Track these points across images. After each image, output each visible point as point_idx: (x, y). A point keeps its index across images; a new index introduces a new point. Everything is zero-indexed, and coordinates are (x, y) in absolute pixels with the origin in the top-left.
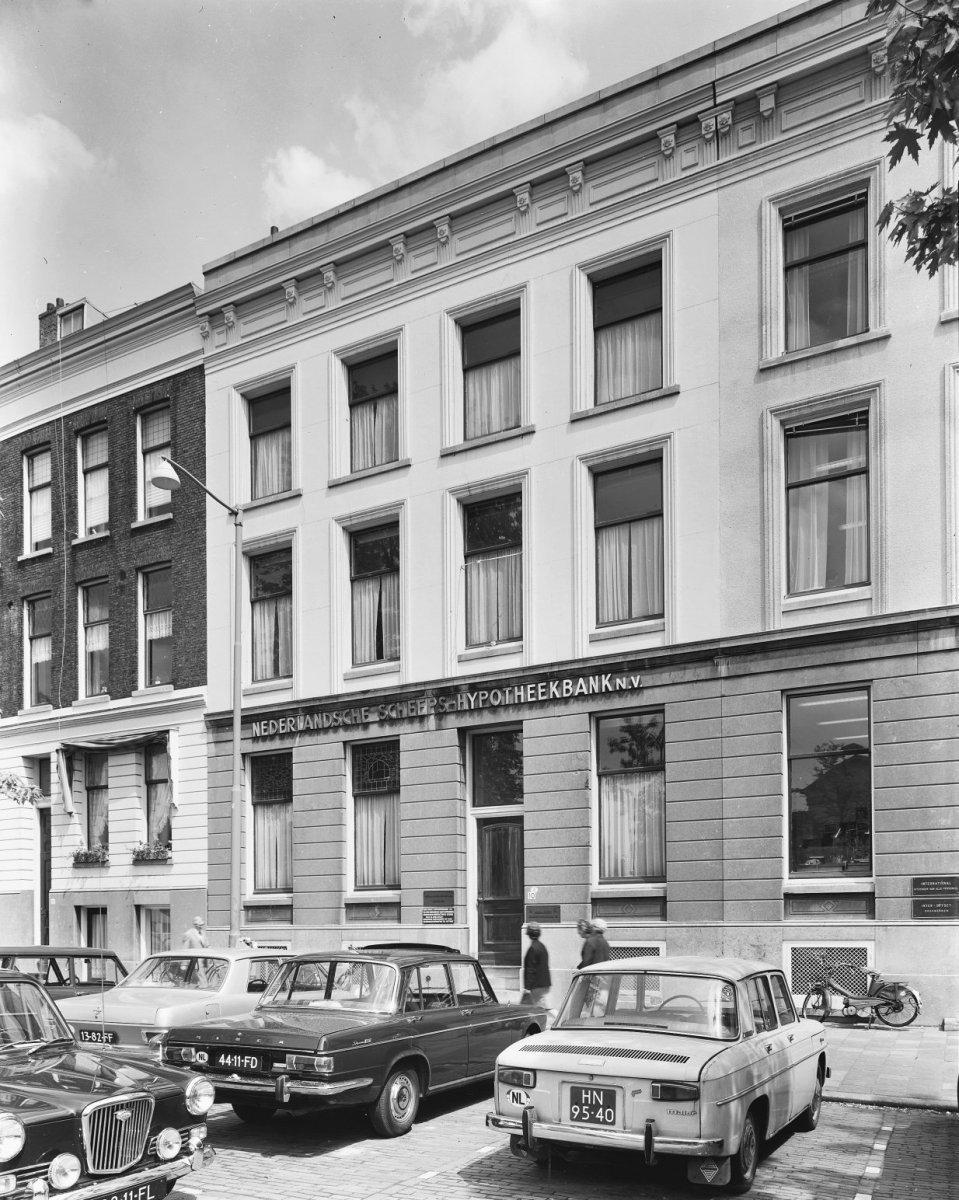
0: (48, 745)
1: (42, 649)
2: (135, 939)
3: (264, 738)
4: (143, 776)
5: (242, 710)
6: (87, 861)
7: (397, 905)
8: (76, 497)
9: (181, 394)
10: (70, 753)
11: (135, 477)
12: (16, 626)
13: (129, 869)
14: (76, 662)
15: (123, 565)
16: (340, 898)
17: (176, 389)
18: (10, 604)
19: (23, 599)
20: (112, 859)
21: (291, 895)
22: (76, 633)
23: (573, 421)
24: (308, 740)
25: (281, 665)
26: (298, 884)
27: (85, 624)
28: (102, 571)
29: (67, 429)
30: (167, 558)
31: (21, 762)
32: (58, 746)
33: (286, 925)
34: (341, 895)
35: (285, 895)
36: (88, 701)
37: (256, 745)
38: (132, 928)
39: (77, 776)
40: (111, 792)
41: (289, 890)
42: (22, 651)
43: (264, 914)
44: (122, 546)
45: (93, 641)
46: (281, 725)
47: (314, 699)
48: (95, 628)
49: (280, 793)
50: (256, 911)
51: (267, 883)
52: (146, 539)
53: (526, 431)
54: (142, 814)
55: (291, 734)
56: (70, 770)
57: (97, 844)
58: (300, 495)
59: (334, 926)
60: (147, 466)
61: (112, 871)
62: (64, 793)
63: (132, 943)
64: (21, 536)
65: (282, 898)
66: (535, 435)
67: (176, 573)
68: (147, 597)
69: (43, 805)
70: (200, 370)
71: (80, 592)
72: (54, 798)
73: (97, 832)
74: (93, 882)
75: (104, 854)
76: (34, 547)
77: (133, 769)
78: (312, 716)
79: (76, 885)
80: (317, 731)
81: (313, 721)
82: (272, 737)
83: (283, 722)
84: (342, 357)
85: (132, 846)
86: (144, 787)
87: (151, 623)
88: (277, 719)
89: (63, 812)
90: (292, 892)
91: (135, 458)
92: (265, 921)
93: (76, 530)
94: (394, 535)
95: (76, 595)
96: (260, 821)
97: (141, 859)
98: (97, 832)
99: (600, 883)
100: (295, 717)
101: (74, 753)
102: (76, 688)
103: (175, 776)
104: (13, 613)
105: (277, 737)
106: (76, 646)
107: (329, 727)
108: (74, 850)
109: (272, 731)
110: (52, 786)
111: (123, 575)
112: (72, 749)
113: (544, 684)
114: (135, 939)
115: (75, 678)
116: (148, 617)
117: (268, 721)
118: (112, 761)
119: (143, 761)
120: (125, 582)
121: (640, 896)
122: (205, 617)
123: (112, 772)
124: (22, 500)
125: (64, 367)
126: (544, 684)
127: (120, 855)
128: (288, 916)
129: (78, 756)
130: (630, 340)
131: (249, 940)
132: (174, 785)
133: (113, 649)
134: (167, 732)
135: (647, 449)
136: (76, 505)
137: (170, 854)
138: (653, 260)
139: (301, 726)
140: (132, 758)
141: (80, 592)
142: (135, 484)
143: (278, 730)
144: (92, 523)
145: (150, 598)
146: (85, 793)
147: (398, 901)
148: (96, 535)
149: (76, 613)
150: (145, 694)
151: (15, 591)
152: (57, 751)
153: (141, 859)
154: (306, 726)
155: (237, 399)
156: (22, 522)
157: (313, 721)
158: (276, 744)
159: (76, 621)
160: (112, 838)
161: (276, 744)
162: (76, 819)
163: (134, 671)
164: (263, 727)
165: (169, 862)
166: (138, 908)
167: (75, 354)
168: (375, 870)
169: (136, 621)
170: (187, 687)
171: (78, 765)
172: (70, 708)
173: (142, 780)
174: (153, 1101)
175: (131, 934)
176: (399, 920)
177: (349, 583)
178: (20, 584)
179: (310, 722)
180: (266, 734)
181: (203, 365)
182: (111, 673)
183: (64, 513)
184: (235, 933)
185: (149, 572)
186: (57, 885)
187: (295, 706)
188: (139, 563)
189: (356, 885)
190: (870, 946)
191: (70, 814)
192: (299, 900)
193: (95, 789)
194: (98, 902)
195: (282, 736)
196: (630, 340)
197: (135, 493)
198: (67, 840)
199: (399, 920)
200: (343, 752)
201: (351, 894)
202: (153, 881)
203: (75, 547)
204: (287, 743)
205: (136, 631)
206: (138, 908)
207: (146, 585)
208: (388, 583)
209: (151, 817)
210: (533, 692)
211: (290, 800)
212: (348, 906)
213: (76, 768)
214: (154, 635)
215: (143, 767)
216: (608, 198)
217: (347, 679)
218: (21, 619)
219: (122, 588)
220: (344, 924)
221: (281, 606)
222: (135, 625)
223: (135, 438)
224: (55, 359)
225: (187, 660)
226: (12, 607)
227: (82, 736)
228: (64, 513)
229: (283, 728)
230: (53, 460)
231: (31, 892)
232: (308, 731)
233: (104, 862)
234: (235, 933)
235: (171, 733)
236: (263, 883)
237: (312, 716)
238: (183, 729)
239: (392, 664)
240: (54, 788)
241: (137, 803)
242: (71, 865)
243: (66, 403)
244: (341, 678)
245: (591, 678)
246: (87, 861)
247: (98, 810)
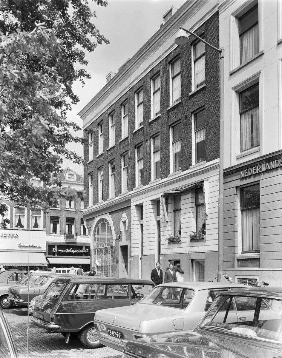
0: (158, 195)
1: (158, 156)
2: (191, 274)
3: (246, 178)
4: (172, 208)
5: (224, 170)
6: (174, 241)
7: (258, 259)
8: (169, 90)
9: (209, 28)
10: (167, 196)
11: (191, 73)
12: (148, 149)
13: (188, 244)
14: (169, 159)
15: (186, 113)
16: (234, 257)
17: (207, 27)
18: (147, 140)
19: (151, 137)
20: (183, 240)
21: (259, 253)
22: (169, 146)
23: (278, 44)
24: (267, 175)
25: (254, 142)
26: (263, 248)
27: (172, 142)
28: (178, 118)
29: (166, 63)
30: (203, 104)
31: (150, 202)
32: (162, 194)
33: (257, 269)
34: (235, 255)
35: (256, 253)
36: (173, 173)
37: (242, 181)
38: (190, 270)
39: (170, 206)
40: (182, 212)
41: (258, 251)
42: (151, 158)
43: (246, 263)
44: (185, 105)
45: (175, 149)
46: (254, 170)
47: (270, 154)
48: (176, 143)
49: (254, 204)
50: (243, 261)
51: (248, 248)
52: (195, 99)
53: (261, 54)
54: (194, 220)
55: (259, 174)
56: (167, 204)
57: (177, 233)
58: (263, 54)
59: (232, 269)
60: (196, 67)
61: (182, 245)
62: (166, 214)
63: (190, 275)
64: (150, 112)
65: (255, 255)
66: (264, 55)
67: (207, 110)
68: (196, 124)
69: (158, 219)
70: (217, 12)
71: (171, 129)
72: (161, 216)
73: (177, 229)
74: (176, 250)
75: (179, 238)
76: (196, 87)
77: (190, 200)
78: (269, 163)
79: (169, 251)
80: (272, 170)
81: (270, 165)
82: (250, 177)
83: (255, 168)
84: (235, 15)
85: (189, 234)
86: (195, 208)
87: (198, 134)
88: (252, 167)
89: (164, 222)
90: (260, 252)
91: (191, 65)
92: (247, 266)
93: (169, 104)
94: (257, 89)
95: (169, 131)
96: (245, 219)
97: (193, 239)
98: (177, 229)
99: (242, 253)
100: (261, 165)
101: (168, 196)
102: (169, 169)
103: (207, 201)
104: (148, 144)
105: (252, 176)
106: (169, 152)
107: (278, 167)
108: (168, 237)
109: (249, 174)
110: (161, 211)
111: (186, 117)
112: (167, 194)
113: (247, 170)
114: (191, 274)
115: (169, 165)
116: (197, 133)
117: (248, 169)
118: (182, 198)
119: (194, 197)
120: (187, 120)
121: (245, 258)
122: (219, 127)
123: (182, 202)
124: (150, 98)
125: (163, 38)
126: (247, 170)
127: (185, 238)
128: (258, 263)
129: (170, 197)
130: (251, 37)
131: (227, 276)
132: (206, 205)
133: (182, 151)
134: (203, 181)
135: (250, 81)
136: (169, 93)
137: (205, 236)
138: (255, 4)
139: (264, 169)
140: (190, 195)
141: (171, 129)
142: (191, 76)
143: (253, 172)
144: (156, 112)
145: (197, 125)
146: (173, 213)
147: (258, 257)
148: (177, 103)
149: (169, 138)
150: (195, 165)
151: (148, 135)
152: (162, 196)
153: (193, 239)
154: (266, 168)
155: (233, 19)
156: (150, 107)
157: (270, 165)
158: (252, 180)
159: (169, 141)
160: (182, 231)
161: (252, 180)
162: (169, 224)
163: (191, 157)
164: (245, 173)
165: (204, 240)
166: (192, 260)
167: (110, 88)
168: (247, 245)
169: (191, 136)
170: (212, 160)
171: (170, 201)
172: (119, 197)
173: (194, 204)
174: (219, 352)
175: (190, 272)
176: (259, 267)
177: (239, 115)
178: (150, 132)
179: (268, 166)
180: (247, 175)
181: (218, 11)
182: (182, 160)
183: (118, 134)
184: (221, 273)
185: (196, 114)
186: (162, 252)
187: (261, 159)
188: (192, 110)
189: (242, 250)
190: (258, 278)
191: (167, 222)
192: (263, 256)
193: (176, 210)
194: (177, 258)
195: (255, 175)
196: (251, 37)
197: (191, 80)
198: (166, 233)
199: (259, 267)
200: (236, 191)
201: (239, 254)
202: (199, 249)
203: (168, 111)
204: (257, 179)
205: (191, 140)
206: (192, 260)
207: (196, 119)
208: (254, 112)
209: (198, 221)
210: (246, 172)
211: (258, 207)
212: (238, 260)
213: (169, 203)
214: (199, 140)
215: (194, 199)
216: (105, 108)
217: (238, 158)
218: (150, 145)
219: (186, 123)
220: (236, 268)
221: (254, 113)
222: (191, 137)
223: (191, 56)
224: (161, 35)
225: (212, 148)
226: (147, 142)
227: (170, 189)
228: (118, 134)
229: (255, 171)
230: (182, 63)
231: (154, 255)
232: (268, 171)
233: (179, 241)
234: (221, 273)
235: (205, 182)
236: (246, 248)
237: (269, 163)
238: (211, 179)
239: (257, 148)
240: (161, 212)
241: (191, 215)
242: (167, 243)
243: (163, 54)
244: (235, 158)
245: (241, 172)
246: (174, 241)
247: (177, 220)
